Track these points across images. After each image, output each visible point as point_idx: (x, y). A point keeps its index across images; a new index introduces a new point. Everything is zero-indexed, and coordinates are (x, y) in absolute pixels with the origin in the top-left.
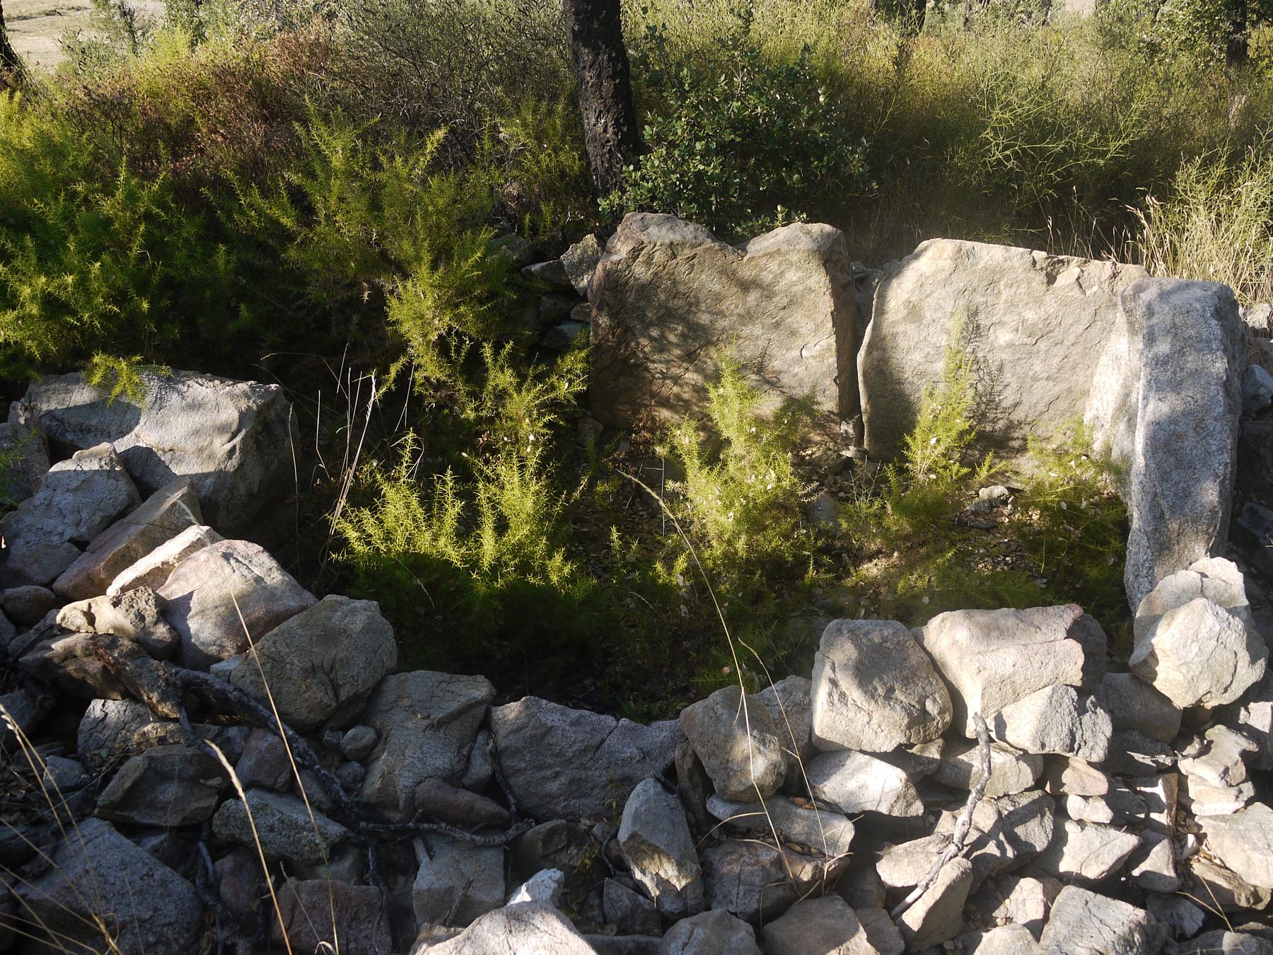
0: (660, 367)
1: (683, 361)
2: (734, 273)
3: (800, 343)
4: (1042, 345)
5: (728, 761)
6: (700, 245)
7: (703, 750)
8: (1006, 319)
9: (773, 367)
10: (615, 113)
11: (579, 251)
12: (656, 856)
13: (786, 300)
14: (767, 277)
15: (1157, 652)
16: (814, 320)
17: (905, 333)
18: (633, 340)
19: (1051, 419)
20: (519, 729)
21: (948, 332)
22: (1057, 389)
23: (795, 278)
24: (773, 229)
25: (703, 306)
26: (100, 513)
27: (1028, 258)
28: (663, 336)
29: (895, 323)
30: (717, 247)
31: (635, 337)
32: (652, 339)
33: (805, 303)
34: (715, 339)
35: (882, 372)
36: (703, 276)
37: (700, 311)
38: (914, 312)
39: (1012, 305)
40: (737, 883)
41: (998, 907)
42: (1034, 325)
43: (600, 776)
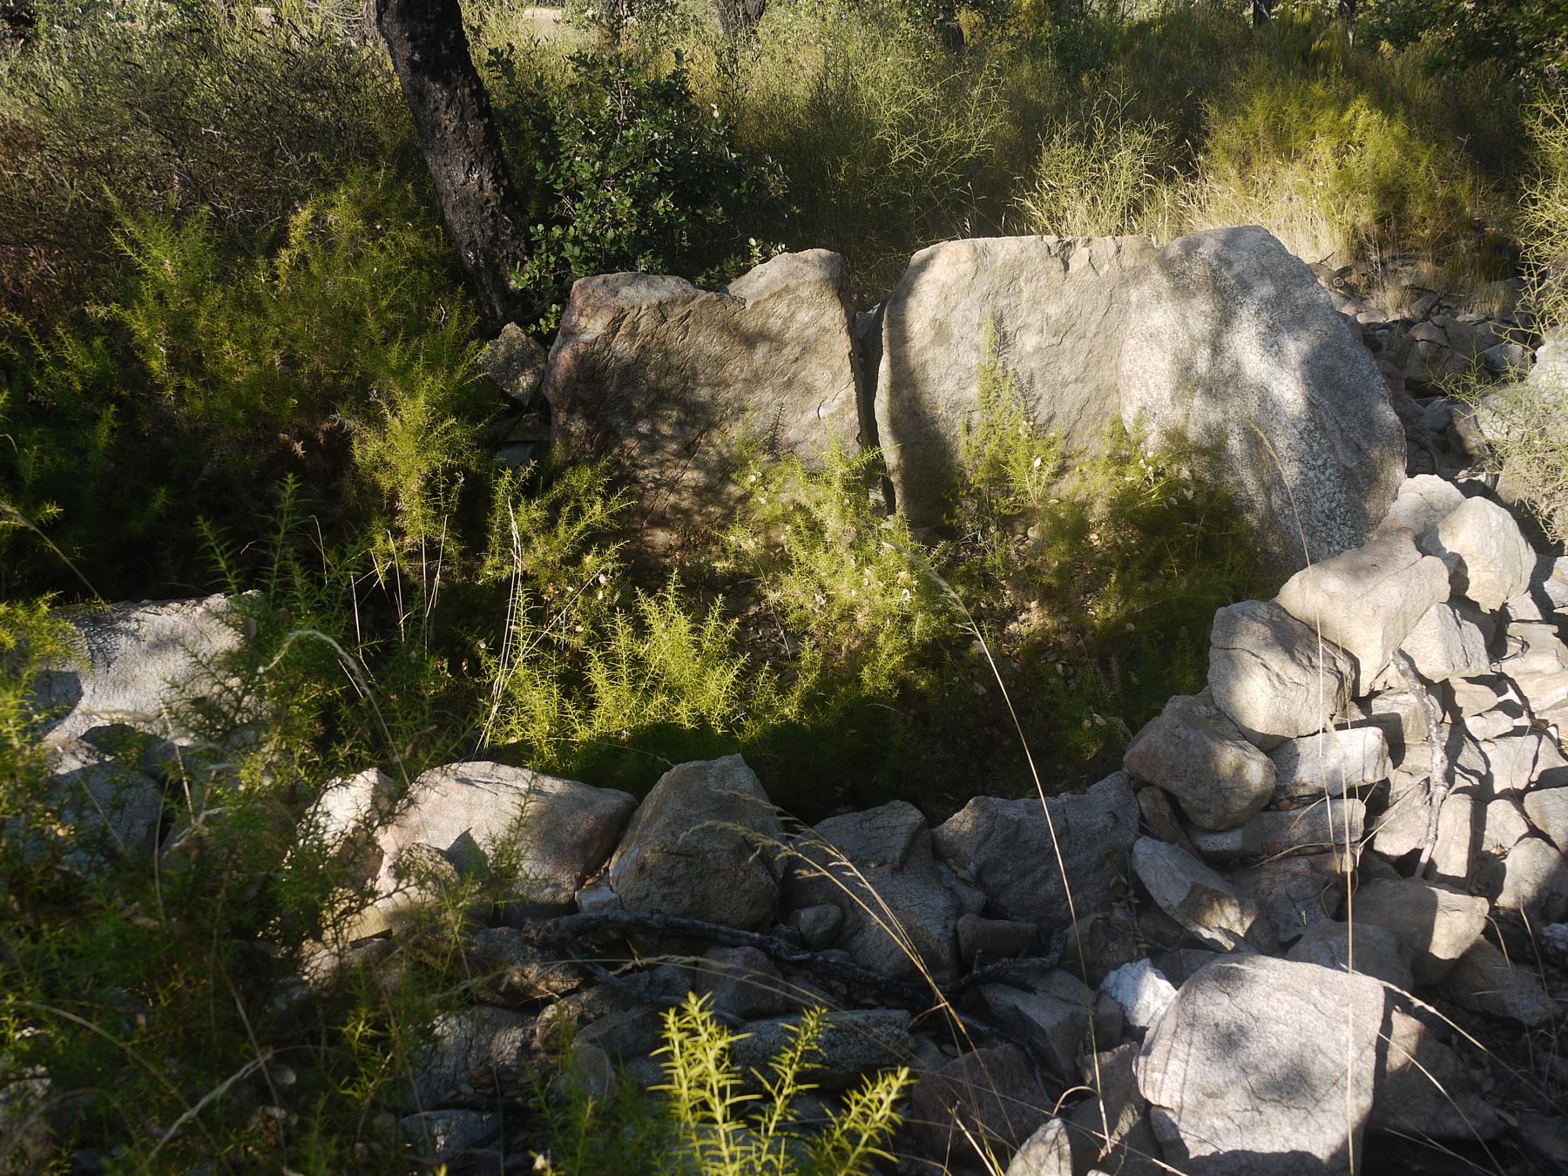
0: (653, 472)
1: (680, 458)
2: (737, 326)
3: (816, 401)
4: (1067, 343)
5: (1219, 781)
6: (694, 298)
7: (1181, 784)
8: (1029, 320)
9: (788, 439)
10: (490, 163)
11: (502, 348)
12: (1216, 905)
13: (798, 350)
14: (775, 324)
15: (1465, 558)
16: (831, 367)
17: (934, 359)
18: (615, 445)
19: (1085, 427)
20: (987, 837)
21: (977, 348)
22: (1086, 390)
23: (806, 319)
24: (749, 268)
25: (702, 379)
26: (142, 821)
27: (1042, 246)
28: (654, 430)
29: (923, 349)
30: (715, 298)
31: (618, 440)
32: (641, 436)
33: (820, 348)
34: (717, 418)
35: (915, 413)
36: (701, 339)
37: (698, 385)
38: (941, 332)
39: (1035, 302)
40: (1290, 903)
41: (1482, 842)
42: (1057, 321)
43: (1088, 859)
